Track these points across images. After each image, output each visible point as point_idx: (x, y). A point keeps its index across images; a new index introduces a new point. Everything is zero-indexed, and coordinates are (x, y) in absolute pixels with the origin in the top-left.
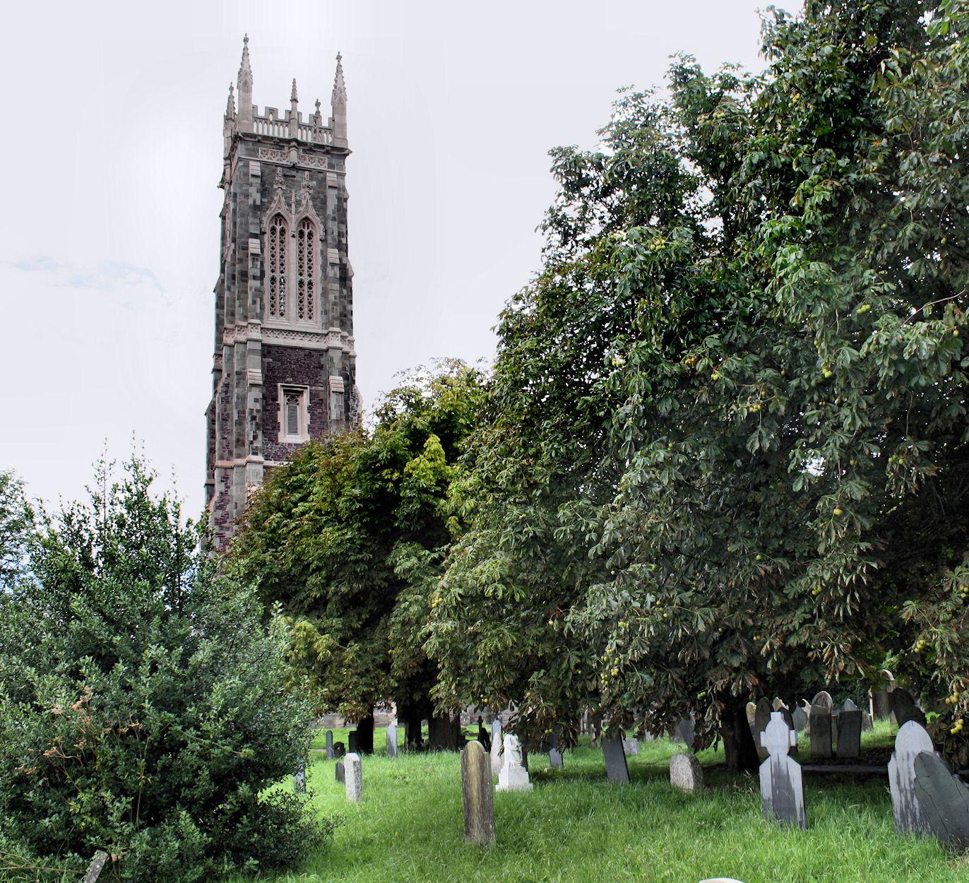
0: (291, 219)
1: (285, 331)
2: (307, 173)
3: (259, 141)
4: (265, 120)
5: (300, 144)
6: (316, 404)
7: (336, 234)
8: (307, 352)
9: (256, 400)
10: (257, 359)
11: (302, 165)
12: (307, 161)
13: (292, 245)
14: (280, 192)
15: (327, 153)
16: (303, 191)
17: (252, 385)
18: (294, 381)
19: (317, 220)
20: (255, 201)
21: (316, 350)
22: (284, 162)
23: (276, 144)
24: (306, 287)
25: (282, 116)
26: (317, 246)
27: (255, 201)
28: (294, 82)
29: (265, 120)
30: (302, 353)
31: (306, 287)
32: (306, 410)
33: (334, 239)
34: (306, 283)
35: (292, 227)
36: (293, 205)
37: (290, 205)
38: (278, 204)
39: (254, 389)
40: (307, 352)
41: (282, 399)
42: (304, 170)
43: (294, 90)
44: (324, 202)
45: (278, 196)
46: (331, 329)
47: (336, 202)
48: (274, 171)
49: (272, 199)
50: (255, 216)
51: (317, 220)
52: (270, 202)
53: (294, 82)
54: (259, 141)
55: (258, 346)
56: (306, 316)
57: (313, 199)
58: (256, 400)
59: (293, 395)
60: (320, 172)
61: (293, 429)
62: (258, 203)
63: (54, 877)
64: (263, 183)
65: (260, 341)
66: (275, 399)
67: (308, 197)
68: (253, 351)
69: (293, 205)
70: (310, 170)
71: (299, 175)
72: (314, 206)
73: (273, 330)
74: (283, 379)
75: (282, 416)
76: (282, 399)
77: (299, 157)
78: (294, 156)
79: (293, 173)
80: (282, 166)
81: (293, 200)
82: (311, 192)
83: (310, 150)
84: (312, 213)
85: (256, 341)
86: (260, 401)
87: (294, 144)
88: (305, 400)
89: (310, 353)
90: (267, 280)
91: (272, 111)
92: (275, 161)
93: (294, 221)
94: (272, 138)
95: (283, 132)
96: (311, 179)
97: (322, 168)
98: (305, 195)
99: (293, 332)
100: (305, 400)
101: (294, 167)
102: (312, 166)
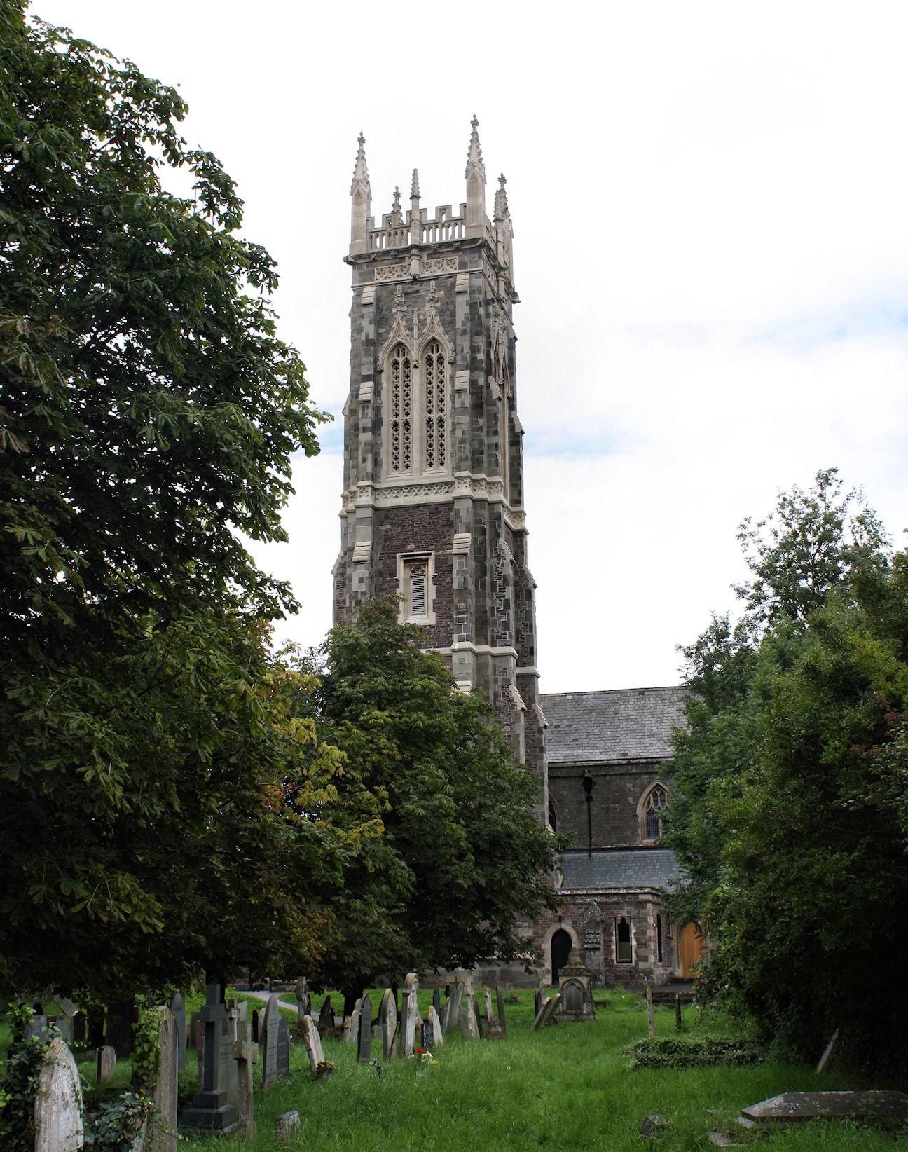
0: (412, 346)
1: (407, 487)
2: (433, 283)
3: (374, 260)
4: (435, 225)
5: (421, 249)
6: (443, 572)
7: (467, 350)
8: (433, 508)
9: (361, 580)
10: (367, 529)
11: (427, 274)
12: (433, 268)
13: (417, 377)
14: (399, 315)
15: (457, 250)
16: (428, 306)
17: (358, 562)
18: (417, 548)
19: (444, 339)
20: (367, 336)
21: (442, 504)
22: (405, 277)
23: (395, 257)
24: (401, 430)
25: (456, 213)
26: (448, 370)
27: (367, 336)
28: (415, 173)
29: (435, 225)
30: (426, 511)
31: (401, 430)
32: (431, 582)
33: (464, 358)
34: (401, 424)
35: (414, 354)
36: (416, 328)
37: (411, 329)
38: (398, 332)
39: (359, 567)
40: (433, 508)
41: (402, 571)
42: (429, 279)
43: (415, 183)
44: (453, 314)
45: (398, 322)
46: (458, 474)
47: (467, 309)
48: (393, 292)
49: (391, 327)
50: (367, 354)
51: (444, 339)
52: (388, 332)
53: (415, 173)
54: (374, 260)
55: (368, 513)
56: (401, 466)
57: (441, 313)
58: (361, 580)
59: (416, 565)
60: (450, 276)
61: (418, 608)
62: (372, 336)
63: (772, 1151)
64: (379, 309)
65: (470, 497)
66: (393, 573)
67: (433, 311)
68: (362, 520)
69: (416, 328)
70: (435, 279)
71: (422, 289)
72: (443, 322)
73: (391, 489)
74: (403, 548)
75: (404, 588)
76: (402, 571)
77: (423, 265)
78: (415, 267)
79: (416, 287)
80: (403, 283)
81: (415, 321)
82: (438, 305)
83: (436, 252)
84: (438, 332)
85: (365, 507)
86: (367, 581)
87: (414, 251)
88: (430, 569)
89: (437, 508)
90: (386, 430)
91: (443, 210)
92: (394, 279)
93: (415, 348)
94: (388, 252)
95: (459, 233)
96: (438, 288)
97: (451, 271)
98: (429, 310)
99: (416, 486)
100: (430, 569)
101: (415, 280)
102: (439, 272)
